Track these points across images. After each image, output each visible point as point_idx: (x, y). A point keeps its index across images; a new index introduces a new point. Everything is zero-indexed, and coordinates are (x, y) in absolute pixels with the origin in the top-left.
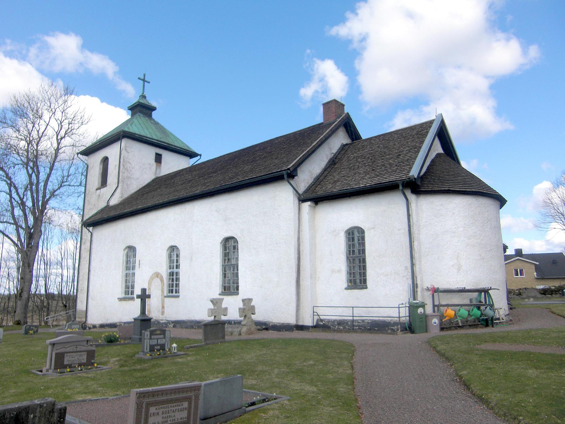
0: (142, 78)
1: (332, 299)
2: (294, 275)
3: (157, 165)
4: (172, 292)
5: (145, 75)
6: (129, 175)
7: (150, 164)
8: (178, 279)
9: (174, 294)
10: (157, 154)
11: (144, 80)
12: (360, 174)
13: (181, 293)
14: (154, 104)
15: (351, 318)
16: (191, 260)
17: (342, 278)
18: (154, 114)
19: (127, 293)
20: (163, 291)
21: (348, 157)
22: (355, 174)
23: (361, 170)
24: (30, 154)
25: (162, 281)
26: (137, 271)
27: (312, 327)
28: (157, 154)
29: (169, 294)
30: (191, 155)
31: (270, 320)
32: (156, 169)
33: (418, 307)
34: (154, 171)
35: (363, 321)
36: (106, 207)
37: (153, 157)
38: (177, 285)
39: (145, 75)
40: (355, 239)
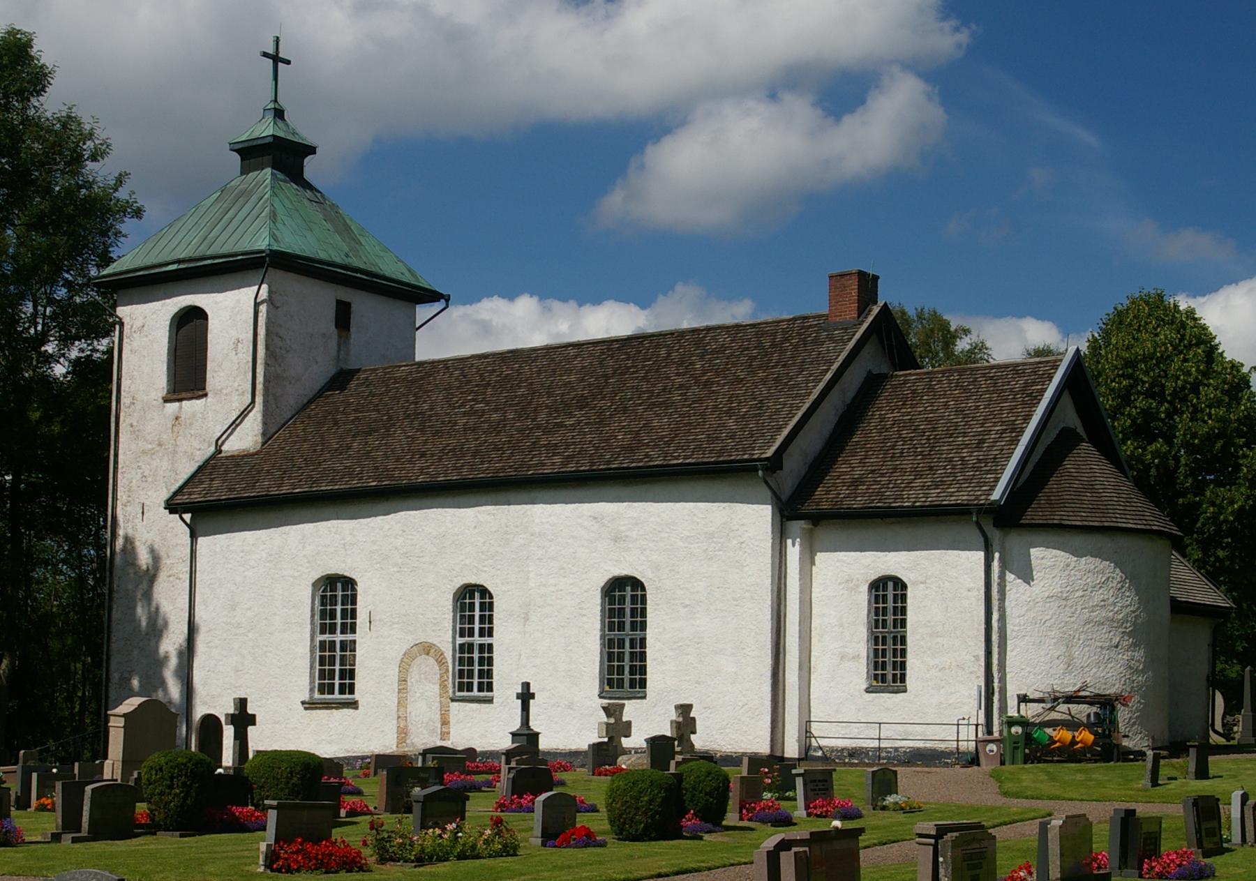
0: (271, 51)
1: (843, 712)
2: (768, 661)
3: (340, 337)
4: (470, 689)
5: (277, 40)
6: (279, 370)
7: (324, 335)
8: (490, 661)
9: (475, 693)
10: (339, 303)
11: (276, 59)
12: (904, 471)
13: (495, 693)
14: (308, 137)
15: (875, 744)
16: (526, 619)
17: (859, 672)
18: (311, 167)
19: (326, 688)
20: (443, 686)
21: (882, 418)
22: (895, 469)
23: (907, 464)
24: (1054, 716)
25: (441, 662)
26: (364, 639)
27: (799, 760)
28: (339, 303)
29: (458, 694)
30: (344, 229)
31: (718, 748)
32: (339, 345)
33: (81, 187)
34: (333, 352)
35: (896, 749)
36: (213, 457)
37: (331, 311)
38: (489, 674)
39: (277, 40)
40: (888, 598)
